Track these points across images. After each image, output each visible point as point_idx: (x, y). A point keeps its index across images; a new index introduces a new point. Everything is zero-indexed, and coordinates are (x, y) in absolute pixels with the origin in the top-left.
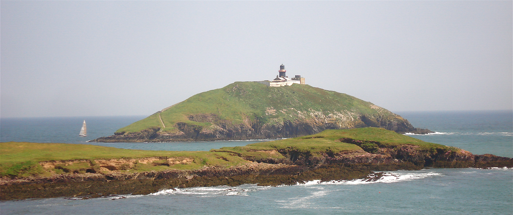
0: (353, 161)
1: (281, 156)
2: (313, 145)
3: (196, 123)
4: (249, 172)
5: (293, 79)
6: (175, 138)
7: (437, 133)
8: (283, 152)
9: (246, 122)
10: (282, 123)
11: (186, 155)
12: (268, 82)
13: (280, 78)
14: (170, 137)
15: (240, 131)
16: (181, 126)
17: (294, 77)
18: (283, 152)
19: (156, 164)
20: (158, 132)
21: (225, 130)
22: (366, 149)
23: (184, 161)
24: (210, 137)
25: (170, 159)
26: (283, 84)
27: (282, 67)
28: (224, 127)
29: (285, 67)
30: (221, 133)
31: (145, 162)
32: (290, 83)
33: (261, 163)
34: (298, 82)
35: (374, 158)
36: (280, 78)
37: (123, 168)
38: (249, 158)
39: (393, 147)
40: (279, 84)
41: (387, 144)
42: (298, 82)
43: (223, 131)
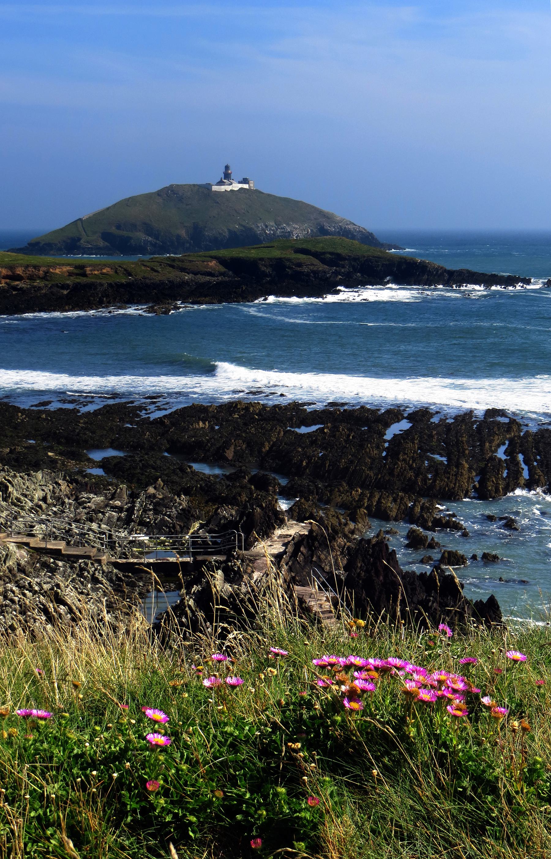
0: (308, 275)
1: (222, 269)
2: (261, 255)
3: (125, 233)
4: (183, 284)
5: (239, 183)
6: (98, 250)
7: (407, 250)
8: (222, 261)
9: (183, 233)
10: (227, 234)
11: (100, 265)
12: (208, 187)
13: (225, 181)
14: (91, 248)
15: (176, 243)
16: (106, 236)
17: (241, 179)
18: (222, 261)
19: (70, 274)
20: (78, 244)
21: (158, 242)
22: (323, 261)
23: (104, 271)
24: (140, 249)
25: (88, 269)
26: (229, 188)
27: (227, 168)
28: (157, 238)
29: (231, 168)
30: (154, 245)
31: (57, 271)
32: (236, 186)
33: (199, 276)
34: (246, 186)
35: (333, 272)
36: (225, 181)
37: (31, 278)
38: (183, 270)
39: (355, 259)
40: (223, 188)
41: (349, 256)
42: (246, 186)
43: (156, 243)
